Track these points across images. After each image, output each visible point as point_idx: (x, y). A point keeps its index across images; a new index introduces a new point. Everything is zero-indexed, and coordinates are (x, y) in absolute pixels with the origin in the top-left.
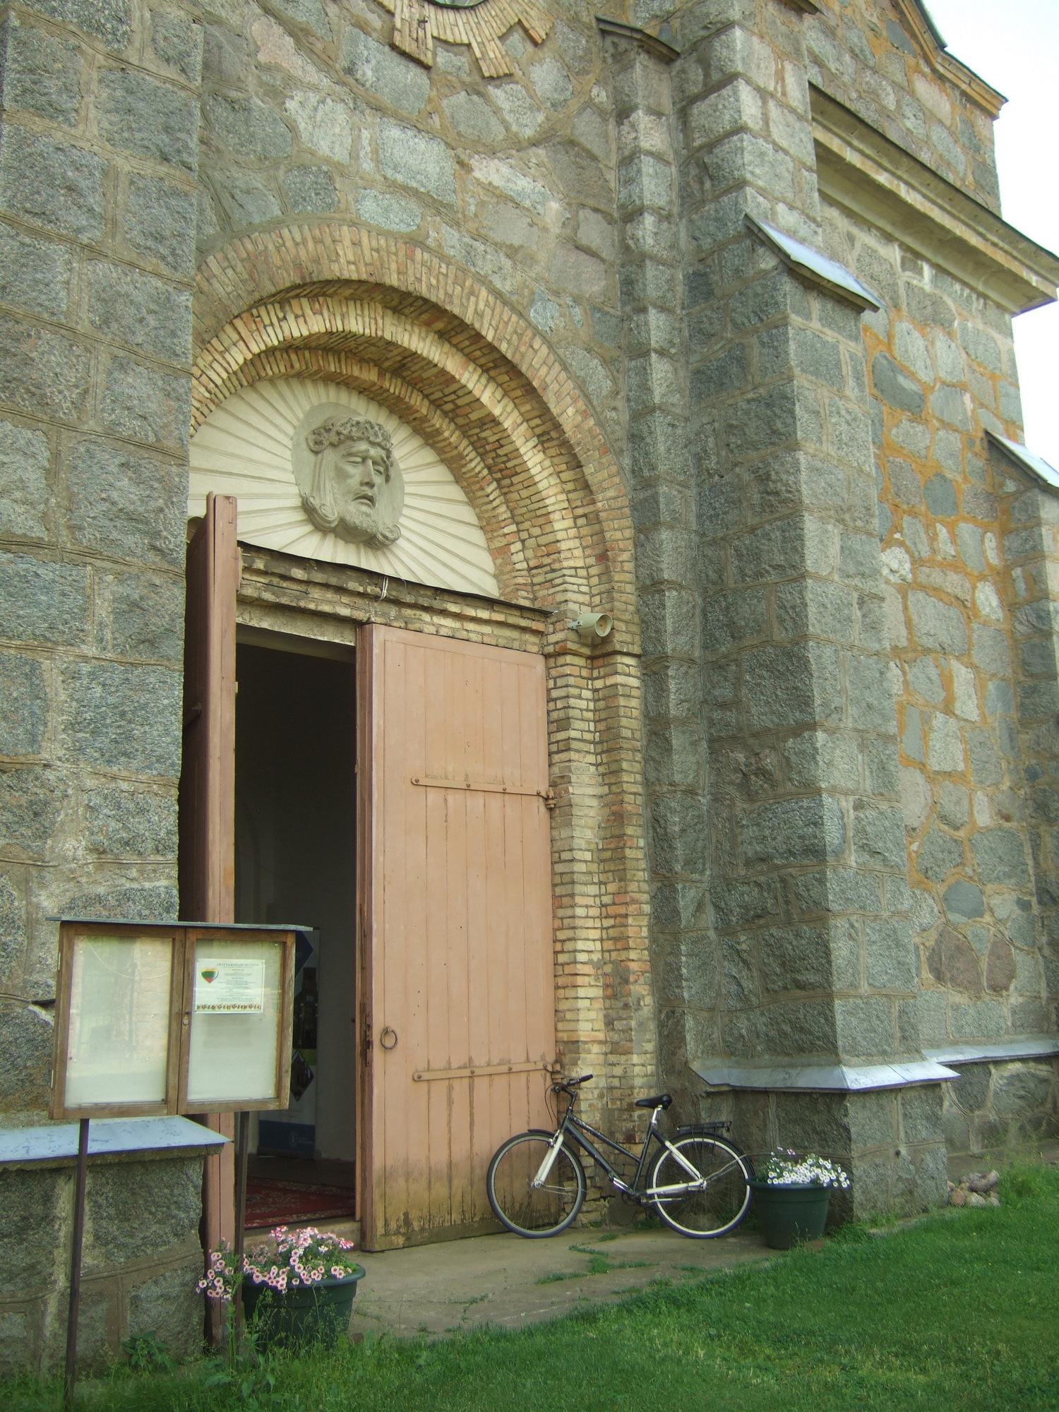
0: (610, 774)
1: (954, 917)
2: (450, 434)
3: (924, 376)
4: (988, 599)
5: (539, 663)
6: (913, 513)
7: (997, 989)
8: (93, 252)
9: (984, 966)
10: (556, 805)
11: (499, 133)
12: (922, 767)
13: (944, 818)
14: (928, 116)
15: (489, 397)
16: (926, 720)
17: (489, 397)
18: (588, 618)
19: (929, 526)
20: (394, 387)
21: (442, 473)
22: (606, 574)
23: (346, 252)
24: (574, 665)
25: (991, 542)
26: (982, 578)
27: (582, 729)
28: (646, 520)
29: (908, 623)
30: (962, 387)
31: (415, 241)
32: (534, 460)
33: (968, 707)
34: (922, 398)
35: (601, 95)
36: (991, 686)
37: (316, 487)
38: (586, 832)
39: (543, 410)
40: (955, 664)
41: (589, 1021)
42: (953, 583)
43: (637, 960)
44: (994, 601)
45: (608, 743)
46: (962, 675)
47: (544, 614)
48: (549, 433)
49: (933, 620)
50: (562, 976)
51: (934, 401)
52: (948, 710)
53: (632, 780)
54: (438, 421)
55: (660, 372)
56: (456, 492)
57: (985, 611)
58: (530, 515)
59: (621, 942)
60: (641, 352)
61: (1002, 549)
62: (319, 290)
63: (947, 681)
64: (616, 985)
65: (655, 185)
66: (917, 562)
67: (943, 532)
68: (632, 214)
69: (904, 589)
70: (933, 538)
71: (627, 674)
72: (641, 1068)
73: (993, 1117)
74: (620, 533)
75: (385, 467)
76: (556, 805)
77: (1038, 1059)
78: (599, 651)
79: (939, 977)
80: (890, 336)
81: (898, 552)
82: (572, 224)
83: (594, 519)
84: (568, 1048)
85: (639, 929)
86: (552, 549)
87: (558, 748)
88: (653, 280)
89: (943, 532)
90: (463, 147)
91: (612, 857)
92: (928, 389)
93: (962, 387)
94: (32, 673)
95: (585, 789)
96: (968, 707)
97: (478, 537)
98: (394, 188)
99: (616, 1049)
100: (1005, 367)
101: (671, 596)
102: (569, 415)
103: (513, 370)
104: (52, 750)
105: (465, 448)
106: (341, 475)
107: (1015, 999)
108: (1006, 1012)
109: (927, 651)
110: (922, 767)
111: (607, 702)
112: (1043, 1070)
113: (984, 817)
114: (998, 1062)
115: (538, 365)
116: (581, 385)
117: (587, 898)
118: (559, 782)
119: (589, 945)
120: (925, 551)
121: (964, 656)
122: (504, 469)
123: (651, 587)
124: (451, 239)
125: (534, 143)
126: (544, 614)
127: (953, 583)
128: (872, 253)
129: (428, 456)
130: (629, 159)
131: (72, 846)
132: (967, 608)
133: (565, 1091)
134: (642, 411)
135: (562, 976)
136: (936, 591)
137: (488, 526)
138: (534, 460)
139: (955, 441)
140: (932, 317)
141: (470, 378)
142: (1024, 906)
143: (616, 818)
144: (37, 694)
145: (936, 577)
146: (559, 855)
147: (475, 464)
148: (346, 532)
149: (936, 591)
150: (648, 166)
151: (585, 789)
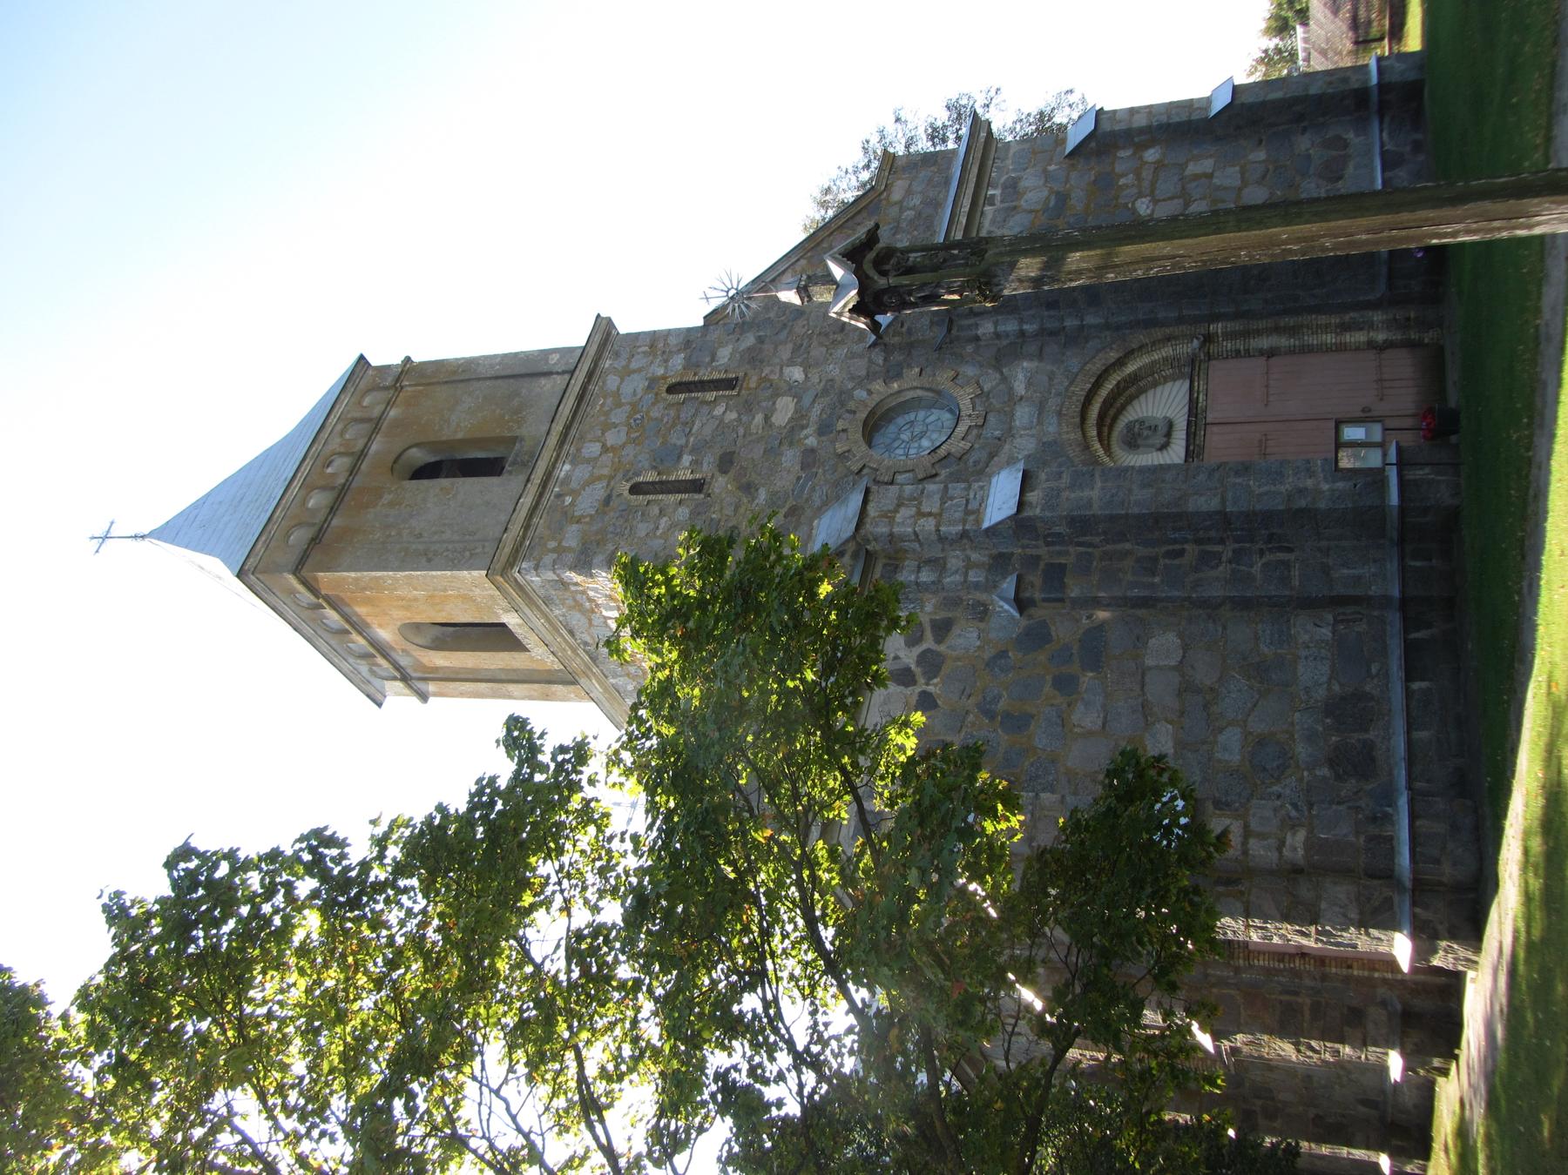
0: (1258, 333)
1: (1312, 171)
2: (1122, 400)
3: (1046, 193)
4: (1151, 155)
5: (1213, 362)
6: (1117, 198)
7: (1346, 145)
8: (1130, 490)
9: (1334, 153)
10: (1271, 353)
11: (1002, 387)
12: (1240, 189)
13: (1264, 177)
14: (909, 192)
15: (1109, 385)
16: (1218, 188)
17: (1109, 385)
18: (1196, 343)
19: (1121, 188)
20: (1108, 421)
21: (1135, 403)
22: (1176, 338)
23: (1072, 436)
24: (1213, 349)
25: (1122, 154)
26: (1141, 158)
27: (1240, 345)
28: (1150, 323)
29: (1171, 198)
30: (1045, 171)
31: (1060, 414)
32: (1131, 368)
33: (1207, 165)
34: (1058, 193)
35: (970, 348)
36: (1195, 152)
37: (1152, 446)
38: (1283, 342)
39: (1113, 364)
40: (1187, 172)
41: (1360, 337)
42: (1147, 174)
43: (1335, 320)
44: (1152, 151)
45: (1246, 334)
46: (1192, 169)
47: (1193, 361)
48: (1120, 363)
49: (1167, 186)
50: (1341, 348)
51: (1057, 187)
52: (1210, 176)
53: (1262, 324)
54: (1118, 405)
55: (1091, 320)
56: (1142, 398)
57: (1158, 156)
58: (1151, 369)
59: (1327, 326)
60: (1082, 327)
61: (1124, 148)
62: (1087, 447)
63: (1196, 177)
64: (1345, 328)
65: (1010, 326)
66: (1140, 195)
67: (1122, 181)
68: (1022, 333)
69: (1155, 201)
70: (1127, 186)
71: (1218, 328)
72: (1377, 317)
73: (1408, 148)
74: (1158, 333)
75: (1141, 422)
76: (1271, 353)
77: (1381, 123)
78: (1208, 339)
79: (1340, 178)
80: (1031, 211)
81: (1138, 204)
82: (1030, 358)
83: (1154, 344)
84: (1371, 345)
85: (1323, 319)
86: (1165, 359)
87: (1248, 354)
88: (1051, 325)
89: (1122, 181)
90: (1012, 400)
91: (1293, 331)
92: (1051, 191)
93: (1045, 171)
94: (1260, 495)
95: (1264, 343)
96: (1207, 165)
97: (1159, 389)
98: (1040, 422)
99: (1371, 326)
100: (1026, 146)
101: (1185, 312)
102: (1113, 355)
103: (1100, 377)
104: (1282, 489)
105: (1128, 393)
106: (1147, 437)
107: (1351, 135)
108: (1357, 140)
109: (1183, 188)
110: (1240, 189)
111: (1229, 336)
112: (1387, 119)
113: (1261, 155)
114: (1382, 146)
115: (1097, 366)
116: (1099, 351)
117: (1312, 340)
118: (1262, 353)
119: (1329, 338)
120: (1135, 190)
121: (1183, 167)
122: (1134, 379)
123: (1181, 320)
124: (1053, 403)
125: (1002, 373)
126: (1193, 361)
127: (1147, 174)
128: (993, 222)
129: (1129, 408)
130: (997, 336)
131: (1309, 483)
132: (1159, 166)
133: (1388, 345)
134: (1107, 326)
135: (1341, 348)
136: (1153, 184)
137: (1155, 385)
138: (1131, 368)
139: (1074, 175)
140: (1012, 188)
141: (1104, 393)
142: (1304, 130)
143: (1277, 330)
144: (1266, 493)
145: (1146, 184)
146: (1291, 351)
147: (1133, 390)
148: (1168, 435)
149: (1153, 184)
150: (1001, 328)
151: (1264, 343)
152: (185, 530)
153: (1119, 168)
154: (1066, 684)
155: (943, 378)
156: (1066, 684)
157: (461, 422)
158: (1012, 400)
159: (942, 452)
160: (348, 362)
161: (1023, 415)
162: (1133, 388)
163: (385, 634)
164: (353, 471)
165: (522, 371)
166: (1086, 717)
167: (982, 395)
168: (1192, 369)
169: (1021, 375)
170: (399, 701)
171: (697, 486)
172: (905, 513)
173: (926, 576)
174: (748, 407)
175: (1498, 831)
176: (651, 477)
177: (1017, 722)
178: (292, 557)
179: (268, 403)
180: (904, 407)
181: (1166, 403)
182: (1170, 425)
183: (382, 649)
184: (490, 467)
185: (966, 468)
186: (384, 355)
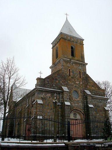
4: (104, 115)
115: (81, 111)
140: (101, 102)
152: (67, 24)
153: (102, 112)
154: (51, 109)
155: (80, 97)
156: (51, 109)
157: (76, 53)
158: (78, 104)
159: (73, 97)
160: (83, 38)
161: (77, 104)
162: (80, 114)
163: (57, 45)
164: (72, 41)
165: (83, 57)
166: (48, 111)
167: (78, 101)
168: (81, 119)
169: (81, 104)
170: (51, 46)
171: (70, 75)
172: (66, 95)
173: (61, 97)
174: (78, 79)
175: (3, 127)
176: (71, 71)
177: (48, 105)
178: (63, 37)
179: (80, 30)
180: (78, 94)
181: (78, 117)
182: (76, 117)
183: (56, 45)
184: (73, 54)
185: (70, 100)
186: (84, 42)
